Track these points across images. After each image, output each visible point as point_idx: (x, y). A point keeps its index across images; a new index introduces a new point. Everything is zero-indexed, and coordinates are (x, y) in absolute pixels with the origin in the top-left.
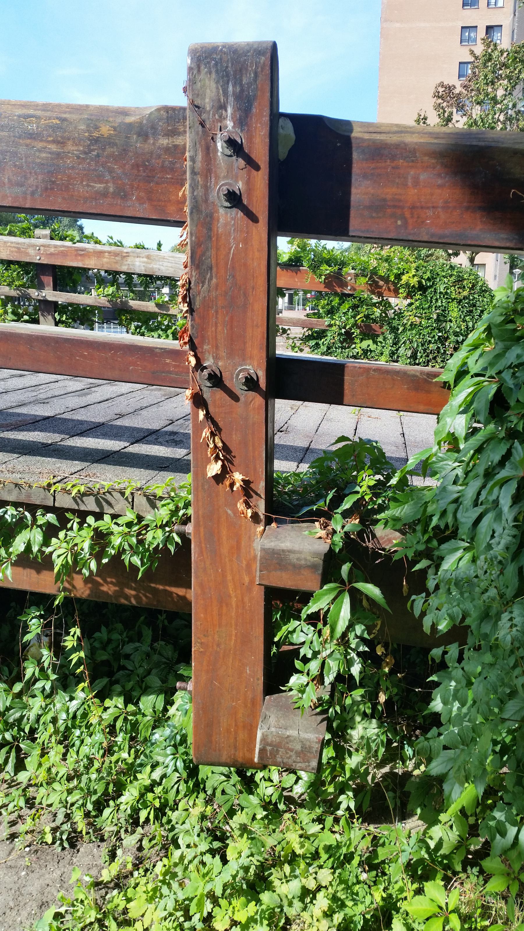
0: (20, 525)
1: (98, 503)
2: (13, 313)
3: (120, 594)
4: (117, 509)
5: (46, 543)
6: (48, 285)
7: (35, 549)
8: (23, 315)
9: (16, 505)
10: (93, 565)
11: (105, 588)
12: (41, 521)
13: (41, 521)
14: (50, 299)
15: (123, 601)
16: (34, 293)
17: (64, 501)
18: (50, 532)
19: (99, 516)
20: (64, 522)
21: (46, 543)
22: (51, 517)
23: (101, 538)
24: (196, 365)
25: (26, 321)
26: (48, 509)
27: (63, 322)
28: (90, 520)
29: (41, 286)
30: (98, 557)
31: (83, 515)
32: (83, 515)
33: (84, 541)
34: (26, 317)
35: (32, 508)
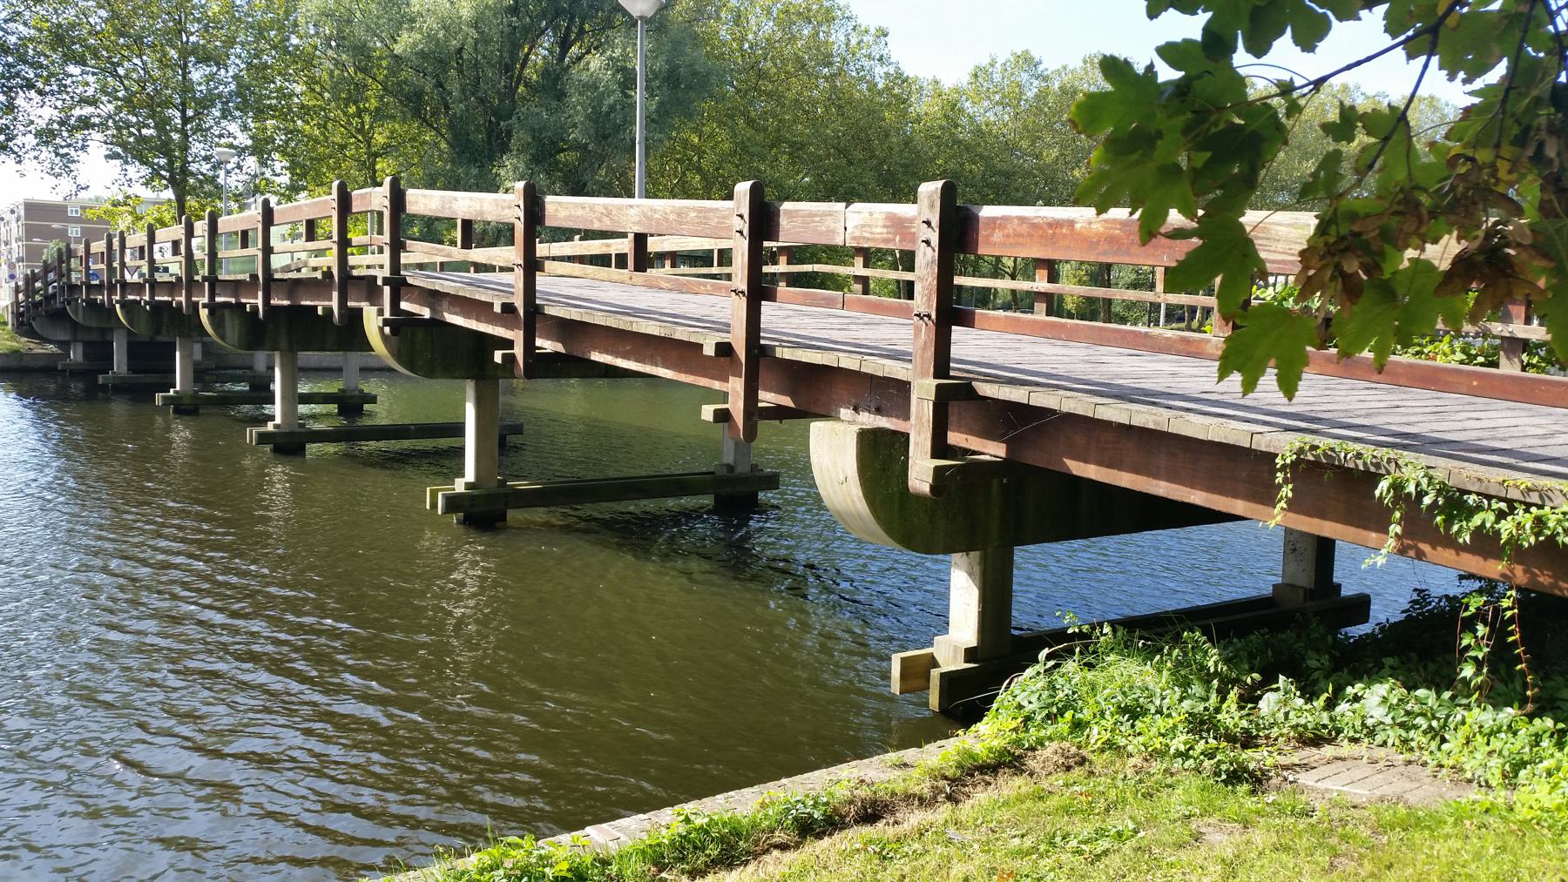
0: (1479, 508)
1: (1541, 497)
2: (1463, 351)
3: (1555, 585)
4: (1556, 503)
5: (1497, 521)
6: (1518, 317)
7: (1488, 525)
8: (1476, 356)
9: (1478, 494)
10: (1532, 540)
11: (1541, 579)
12: (1495, 506)
13: (1495, 506)
14: (1520, 335)
15: (1557, 592)
16: (1497, 328)
17: (1514, 494)
18: (1501, 515)
19: (1541, 507)
20: (1512, 509)
21: (1497, 521)
22: (1503, 505)
23: (1540, 522)
24: (973, 391)
25: (1482, 365)
26: (1501, 499)
27: (1534, 366)
28: (1533, 509)
29: (1506, 319)
30: (1537, 535)
31: (1528, 506)
32: (1528, 506)
33: (1527, 520)
34: (1481, 359)
35: (1489, 497)
